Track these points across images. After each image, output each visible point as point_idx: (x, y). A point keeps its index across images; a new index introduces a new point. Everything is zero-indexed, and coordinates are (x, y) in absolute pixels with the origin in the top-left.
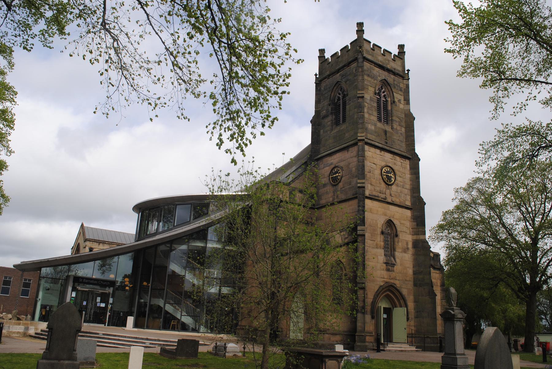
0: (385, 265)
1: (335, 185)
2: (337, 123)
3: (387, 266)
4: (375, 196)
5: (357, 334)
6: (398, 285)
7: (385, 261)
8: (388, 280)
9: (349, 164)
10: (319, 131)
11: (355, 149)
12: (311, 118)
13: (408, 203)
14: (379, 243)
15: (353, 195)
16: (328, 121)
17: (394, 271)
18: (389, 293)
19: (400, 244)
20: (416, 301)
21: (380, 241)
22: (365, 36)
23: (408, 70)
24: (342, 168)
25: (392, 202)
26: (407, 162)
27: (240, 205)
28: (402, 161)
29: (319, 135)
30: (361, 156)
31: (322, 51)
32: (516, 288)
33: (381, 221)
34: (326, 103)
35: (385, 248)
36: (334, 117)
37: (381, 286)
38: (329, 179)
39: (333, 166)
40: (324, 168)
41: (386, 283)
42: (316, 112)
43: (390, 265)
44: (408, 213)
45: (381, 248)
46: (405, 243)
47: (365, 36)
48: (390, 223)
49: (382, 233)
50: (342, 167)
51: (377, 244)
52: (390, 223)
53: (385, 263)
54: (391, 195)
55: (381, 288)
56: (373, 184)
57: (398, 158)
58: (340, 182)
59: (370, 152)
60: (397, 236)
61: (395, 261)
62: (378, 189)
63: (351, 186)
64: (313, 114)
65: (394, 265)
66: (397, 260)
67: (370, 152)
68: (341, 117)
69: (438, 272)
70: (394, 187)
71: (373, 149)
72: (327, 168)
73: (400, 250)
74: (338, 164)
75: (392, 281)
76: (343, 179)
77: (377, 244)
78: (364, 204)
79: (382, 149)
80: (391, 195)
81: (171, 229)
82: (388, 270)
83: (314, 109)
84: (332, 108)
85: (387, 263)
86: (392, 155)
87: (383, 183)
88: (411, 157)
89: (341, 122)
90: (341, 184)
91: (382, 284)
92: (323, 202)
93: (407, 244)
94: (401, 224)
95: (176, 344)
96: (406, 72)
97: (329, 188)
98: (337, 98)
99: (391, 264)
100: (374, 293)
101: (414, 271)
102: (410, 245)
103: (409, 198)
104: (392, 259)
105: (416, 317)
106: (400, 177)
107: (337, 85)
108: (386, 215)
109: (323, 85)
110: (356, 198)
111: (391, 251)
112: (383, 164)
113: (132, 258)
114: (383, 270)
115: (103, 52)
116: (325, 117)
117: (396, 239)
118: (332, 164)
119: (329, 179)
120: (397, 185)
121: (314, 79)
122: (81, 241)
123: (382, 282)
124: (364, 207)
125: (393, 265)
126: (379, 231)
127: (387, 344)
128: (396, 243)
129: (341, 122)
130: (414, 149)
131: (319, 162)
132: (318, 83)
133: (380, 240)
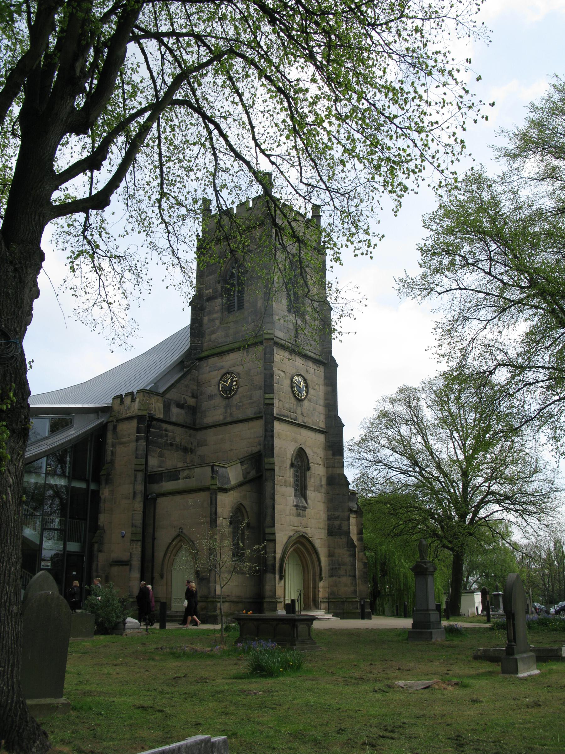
0: (294, 508)
1: (228, 398)
2: (229, 309)
4: (284, 416)
5: (266, 600)
6: (310, 535)
7: (295, 503)
8: (298, 529)
9: (250, 370)
10: (202, 318)
11: (260, 349)
13: (322, 425)
14: (288, 479)
15: (255, 413)
17: (305, 516)
18: (300, 546)
19: (312, 480)
20: (331, 555)
21: (290, 477)
24: (238, 375)
26: (322, 369)
27: (93, 423)
28: (315, 367)
29: (201, 325)
30: (268, 359)
34: (211, 279)
35: (295, 485)
38: (219, 388)
39: (224, 371)
40: (209, 372)
41: (297, 532)
43: (300, 509)
44: (321, 438)
45: (290, 486)
46: (318, 479)
48: (301, 454)
49: (292, 465)
50: (239, 374)
51: (286, 481)
52: (301, 454)
54: (302, 414)
56: (282, 399)
57: (311, 364)
58: (235, 394)
59: (279, 356)
60: (309, 468)
61: (307, 502)
62: (287, 406)
63: (252, 401)
65: (305, 507)
66: (309, 501)
67: (279, 356)
68: (236, 301)
70: (306, 403)
71: (281, 352)
72: (215, 373)
73: (313, 489)
74: (233, 369)
75: (303, 529)
76: (240, 390)
77: (286, 481)
78: (273, 427)
80: (302, 414)
82: (299, 515)
87: (293, 399)
88: (325, 361)
89: (236, 309)
90: (237, 397)
91: (291, 533)
92: (209, 420)
94: (314, 453)
96: (322, 244)
97: (218, 401)
98: (229, 273)
101: (328, 516)
103: (322, 417)
104: (304, 501)
105: (331, 576)
106: (314, 389)
108: (296, 442)
110: (260, 418)
112: (293, 371)
114: (293, 515)
115: (416, 162)
118: (222, 368)
119: (219, 388)
120: (310, 401)
124: (273, 431)
125: (305, 508)
127: (242, 573)
128: (308, 479)
129: (236, 309)
130: (330, 352)
131: (202, 362)
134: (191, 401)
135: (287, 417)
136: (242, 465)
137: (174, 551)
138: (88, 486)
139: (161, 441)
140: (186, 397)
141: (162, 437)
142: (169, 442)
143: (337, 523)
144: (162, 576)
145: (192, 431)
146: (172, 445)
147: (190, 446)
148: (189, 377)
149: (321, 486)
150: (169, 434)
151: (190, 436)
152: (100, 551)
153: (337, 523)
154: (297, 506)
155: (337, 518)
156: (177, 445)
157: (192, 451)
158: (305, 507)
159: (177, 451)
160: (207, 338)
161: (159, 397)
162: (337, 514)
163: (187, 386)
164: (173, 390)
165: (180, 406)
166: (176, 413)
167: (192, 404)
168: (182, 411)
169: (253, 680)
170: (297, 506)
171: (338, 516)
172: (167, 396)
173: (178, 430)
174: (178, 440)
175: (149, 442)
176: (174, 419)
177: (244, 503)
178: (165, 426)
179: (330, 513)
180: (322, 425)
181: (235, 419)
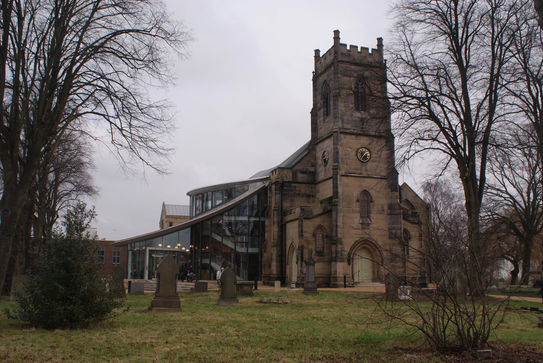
3: (362, 225)
7: (361, 222)
12: (311, 110)
16: (321, 113)
19: (375, 207)
22: (342, 41)
23: (386, 60)
25: (367, 176)
27: (260, 185)
29: (316, 124)
31: (317, 52)
32: (377, 251)
33: (356, 193)
34: (319, 97)
36: (325, 109)
37: (357, 241)
41: (362, 238)
42: (314, 105)
44: (384, 182)
47: (342, 41)
48: (365, 193)
49: (358, 201)
52: (365, 193)
53: (361, 223)
55: (357, 243)
60: (372, 202)
64: (312, 107)
66: (372, 220)
69: (416, 226)
70: (370, 164)
77: (353, 210)
79: (357, 135)
81: (205, 212)
83: (312, 103)
84: (323, 102)
85: (362, 224)
86: (368, 138)
91: (358, 239)
93: (383, 207)
95: (208, 289)
99: (367, 224)
100: (350, 247)
102: (386, 208)
107: (325, 83)
108: (361, 187)
109: (321, 79)
111: (368, 213)
113: (318, 174)
116: (320, 109)
117: (372, 204)
121: (311, 76)
122: (164, 218)
123: (358, 237)
126: (355, 200)
132: (315, 79)
133: (356, 207)
134: (312, 169)
135: (351, 173)
136: (321, 204)
137: (292, 252)
138: (260, 219)
139: (291, 193)
140: (307, 167)
141: (292, 191)
142: (297, 193)
143: (394, 231)
144: (288, 264)
145: (313, 185)
146: (299, 194)
147: (311, 194)
148: (309, 156)
149: (383, 210)
150: (297, 189)
151: (311, 188)
152: (265, 252)
153: (394, 231)
154: (362, 224)
155: (394, 228)
156: (302, 194)
157: (313, 196)
158: (369, 224)
159: (303, 197)
160: (319, 131)
161: (288, 170)
162: (394, 226)
163: (308, 161)
164: (298, 165)
165: (303, 172)
166: (301, 177)
167: (312, 170)
168: (306, 175)
169: (198, 294)
170: (362, 224)
171: (395, 227)
172: (294, 169)
173: (303, 186)
174: (303, 191)
175: (282, 195)
176: (300, 180)
177: (323, 224)
178: (293, 185)
179: (390, 226)
180: (384, 174)
181: (328, 177)
